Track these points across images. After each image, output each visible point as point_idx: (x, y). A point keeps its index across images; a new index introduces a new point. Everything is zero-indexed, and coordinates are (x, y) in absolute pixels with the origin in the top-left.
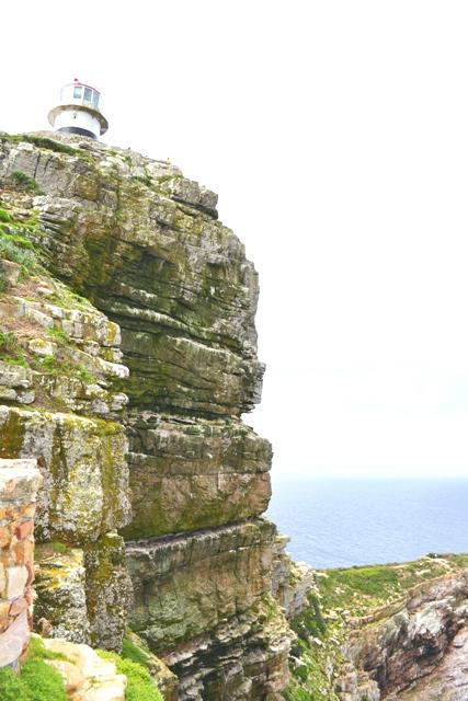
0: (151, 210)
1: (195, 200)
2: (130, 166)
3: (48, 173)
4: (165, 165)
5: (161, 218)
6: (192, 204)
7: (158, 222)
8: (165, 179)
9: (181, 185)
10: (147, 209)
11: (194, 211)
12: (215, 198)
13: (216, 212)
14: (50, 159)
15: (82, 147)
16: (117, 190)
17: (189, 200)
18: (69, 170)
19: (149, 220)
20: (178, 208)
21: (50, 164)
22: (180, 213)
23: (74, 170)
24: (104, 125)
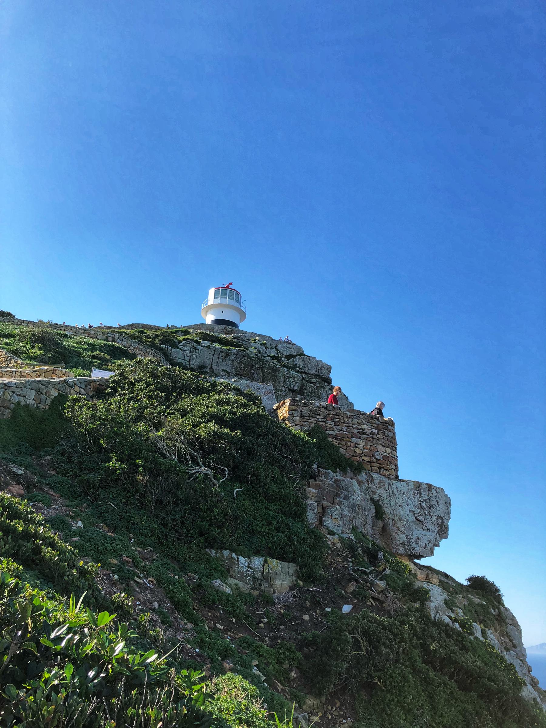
0: (284, 381)
1: (314, 371)
2: (266, 348)
3: (221, 360)
4: (290, 346)
5: (292, 386)
6: (312, 375)
7: (289, 389)
8: (289, 357)
9: (303, 361)
10: (282, 380)
11: (314, 380)
12: (329, 369)
13: (330, 379)
14: (222, 351)
15: (234, 338)
16: (262, 369)
17: (310, 372)
18: (233, 358)
19: (283, 389)
20: (303, 378)
21: (221, 354)
22: (304, 382)
23: (236, 357)
24: (243, 315)
